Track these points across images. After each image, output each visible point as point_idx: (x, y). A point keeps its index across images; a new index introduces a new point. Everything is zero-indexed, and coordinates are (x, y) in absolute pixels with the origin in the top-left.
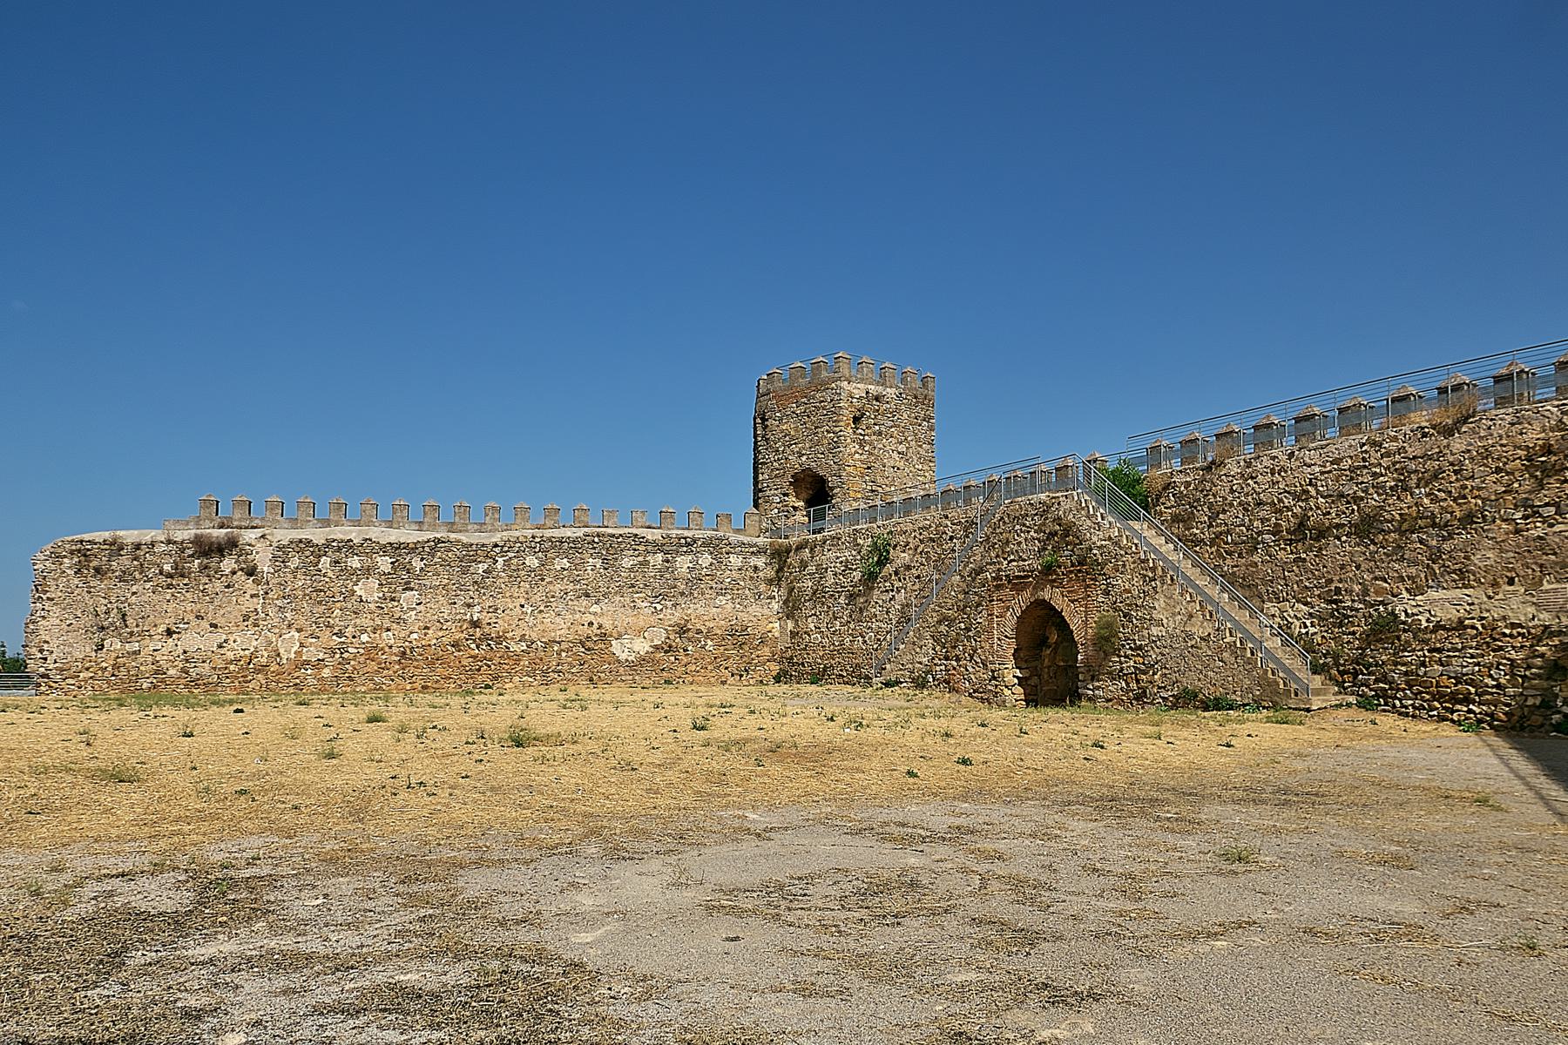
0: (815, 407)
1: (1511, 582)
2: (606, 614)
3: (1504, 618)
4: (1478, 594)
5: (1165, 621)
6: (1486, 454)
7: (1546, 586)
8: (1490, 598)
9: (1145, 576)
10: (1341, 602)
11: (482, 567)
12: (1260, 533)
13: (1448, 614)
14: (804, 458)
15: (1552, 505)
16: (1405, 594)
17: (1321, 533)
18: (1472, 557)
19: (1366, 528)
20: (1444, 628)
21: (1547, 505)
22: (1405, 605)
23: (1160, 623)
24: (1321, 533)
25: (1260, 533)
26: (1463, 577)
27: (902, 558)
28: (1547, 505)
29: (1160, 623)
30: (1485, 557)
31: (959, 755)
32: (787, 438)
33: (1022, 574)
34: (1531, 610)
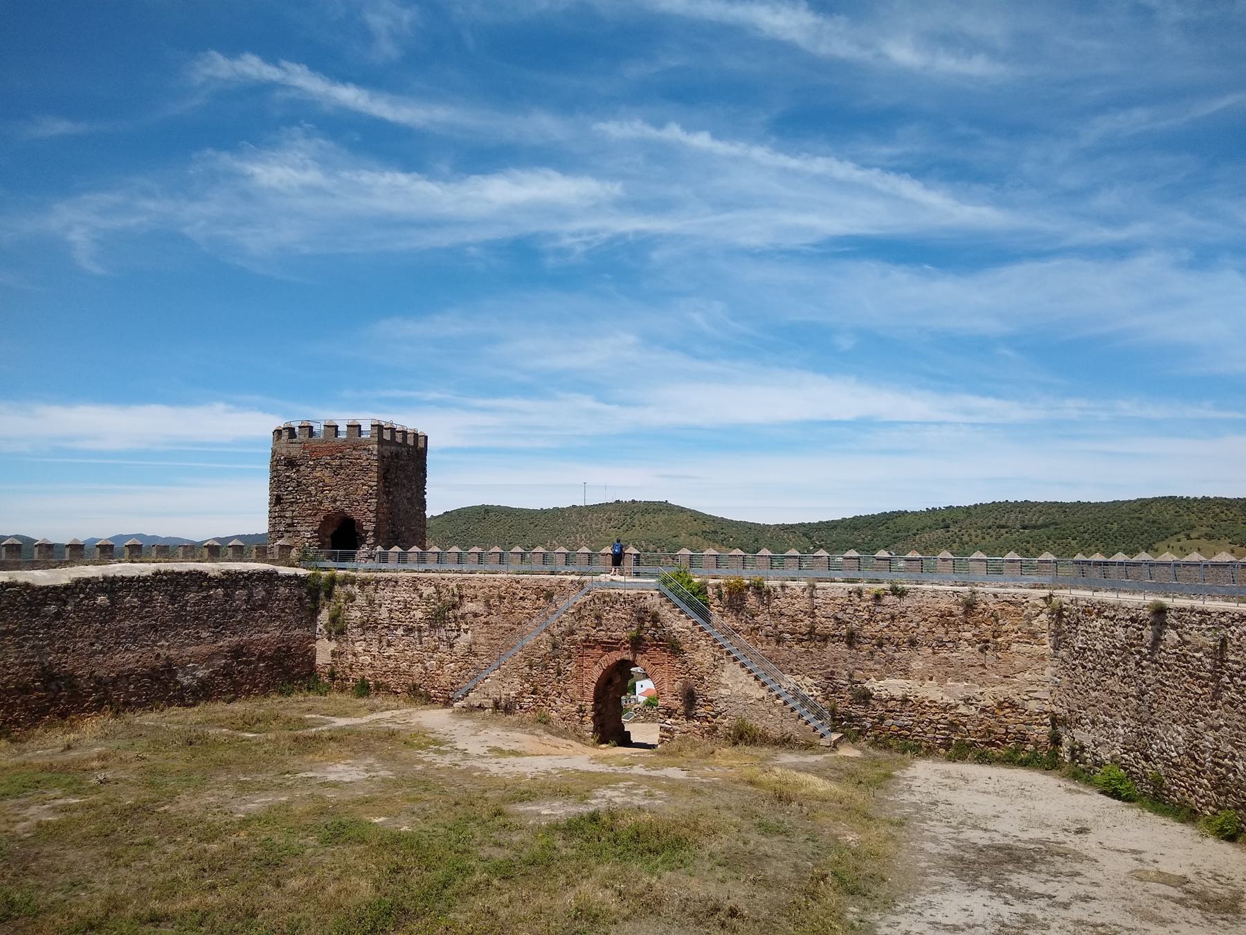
0: (913, 720)
1: (931, 679)
2: (166, 648)
3: (927, 697)
4: (913, 684)
5: (730, 685)
6: (919, 610)
7: (949, 683)
8: (921, 686)
9: (715, 656)
10: (834, 679)
11: (53, 608)
12: (782, 632)
13: (898, 693)
14: (338, 503)
15: (953, 642)
16: (873, 679)
17: (825, 639)
18: (911, 664)
19: (851, 639)
20: (895, 699)
21: (949, 642)
22: (873, 685)
23: (726, 686)
24: (825, 639)
25: (782, 632)
26: (906, 673)
27: (470, 607)
28: (949, 642)
29: (726, 686)
30: (917, 665)
31: (1065, 888)
32: (321, 484)
33: (610, 640)
34: (940, 694)
